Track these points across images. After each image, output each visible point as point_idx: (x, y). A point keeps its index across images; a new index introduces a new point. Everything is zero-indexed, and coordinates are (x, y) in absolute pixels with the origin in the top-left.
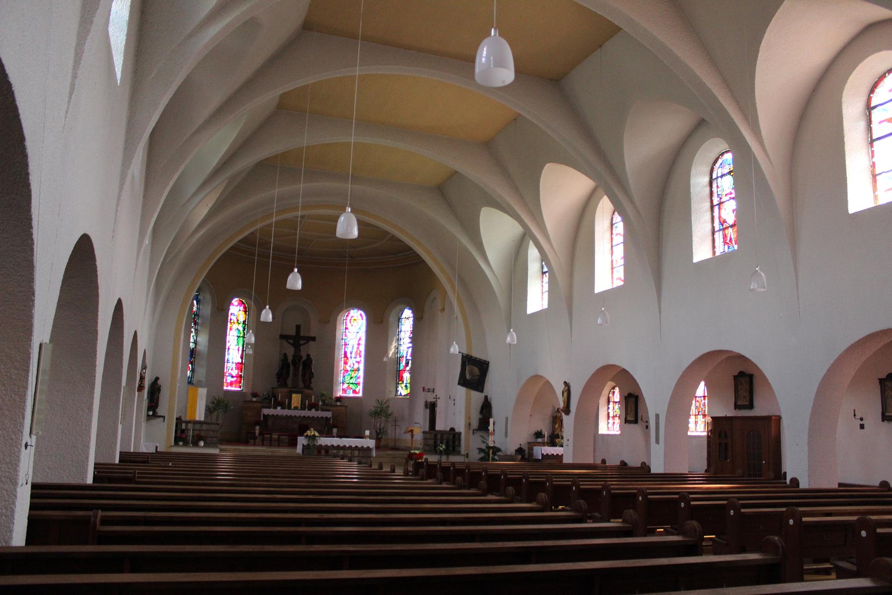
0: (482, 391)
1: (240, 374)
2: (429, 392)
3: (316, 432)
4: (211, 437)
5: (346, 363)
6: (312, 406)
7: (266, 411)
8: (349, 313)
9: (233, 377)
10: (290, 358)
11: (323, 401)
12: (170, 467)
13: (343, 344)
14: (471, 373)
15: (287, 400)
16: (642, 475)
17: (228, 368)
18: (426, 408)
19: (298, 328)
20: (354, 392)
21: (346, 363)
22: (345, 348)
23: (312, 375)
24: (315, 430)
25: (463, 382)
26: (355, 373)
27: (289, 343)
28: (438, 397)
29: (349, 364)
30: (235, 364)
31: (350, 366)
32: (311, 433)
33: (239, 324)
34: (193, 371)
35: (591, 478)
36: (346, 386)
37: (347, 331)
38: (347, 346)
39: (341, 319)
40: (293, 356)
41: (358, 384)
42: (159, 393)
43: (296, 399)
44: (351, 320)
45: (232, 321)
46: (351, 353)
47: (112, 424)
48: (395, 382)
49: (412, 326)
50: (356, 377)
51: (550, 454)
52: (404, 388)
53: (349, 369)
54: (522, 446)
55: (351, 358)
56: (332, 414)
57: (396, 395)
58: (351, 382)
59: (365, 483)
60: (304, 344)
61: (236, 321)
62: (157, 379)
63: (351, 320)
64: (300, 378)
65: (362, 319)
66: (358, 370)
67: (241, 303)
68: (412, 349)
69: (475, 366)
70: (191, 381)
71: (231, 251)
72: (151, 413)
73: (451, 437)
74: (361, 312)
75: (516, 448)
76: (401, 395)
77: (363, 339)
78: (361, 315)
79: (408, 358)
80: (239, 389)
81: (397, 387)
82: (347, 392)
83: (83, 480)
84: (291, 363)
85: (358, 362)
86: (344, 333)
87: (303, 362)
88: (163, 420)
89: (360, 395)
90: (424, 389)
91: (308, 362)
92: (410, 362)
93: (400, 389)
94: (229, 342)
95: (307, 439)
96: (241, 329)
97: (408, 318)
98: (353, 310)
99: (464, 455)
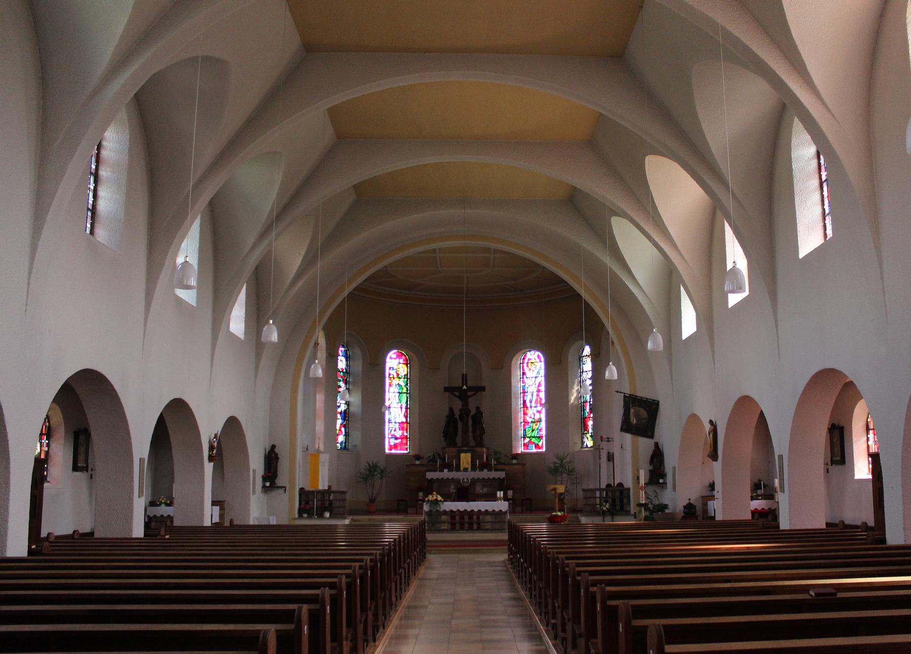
0: (652, 437)
1: (405, 434)
3: (439, 496)
4: (338, 507)
5: (525, 414)
6: (482, 467)
7: (430, 475)
8: (525, 356)
9: (396, 438)
10: (457, 414)
11: (497, 460)
12: (167, 539)
13: (522, 392)
14: (637, 415)
15: (454, 461)
17: (391, 429)
19: (464, 378)
20: (537, 446)
21: (525, 414)
23: (483, 431)
24: (439, 493)
25: (627, 427)
26: (536, 425)
27: (455, 396)
28: (601, 447)
29: (529, 415)
30: (398, 424)
31: (530, 417)
32: (433, 497)
33: (400, 378)
34: (346, 435)
35: (663, 538)
36: (527, 440)
37: (525, 376)
38: (526, 394)
39: (516, 362)
41: (540, 437)
42: (277, 462)
43: (466, 459)
44: (528, 363)
45: (391, 376)
46: (531, 402)
50: (538, 429)
51: (165, 516)
53: (529, 420)
54: (691, 502)
55: (531, 407)
57: (582, 448)
58: (533, 435)
59: (351, 550)
61: (395, 376)
62: (273, 447)
63: (528, 363)
64: (471, 434)
65: (541, 361)
66: (540, 420)
67: (400, 354)
69: (641, 407)
70: (346, 445)
72: (268, 484)
73: (618, 494)
74: (537, 353)
75: (685, 504)
76: (587, 447)
77: (543, 383)
78: (538, 356)
80: (406, 452)
81: (582, 438)
82: (529, 448)
83: (3, 555)
84: (458, 418)
85: (539, 412)
86: (521, 379)
87: (472, 416)
88: (283, 491)
91: (478, 418)
93: (585, 440)
94: (389, 399)
95: (429, 504)
96: (403, 384)
98: (530, 351)
99: (632, 515)
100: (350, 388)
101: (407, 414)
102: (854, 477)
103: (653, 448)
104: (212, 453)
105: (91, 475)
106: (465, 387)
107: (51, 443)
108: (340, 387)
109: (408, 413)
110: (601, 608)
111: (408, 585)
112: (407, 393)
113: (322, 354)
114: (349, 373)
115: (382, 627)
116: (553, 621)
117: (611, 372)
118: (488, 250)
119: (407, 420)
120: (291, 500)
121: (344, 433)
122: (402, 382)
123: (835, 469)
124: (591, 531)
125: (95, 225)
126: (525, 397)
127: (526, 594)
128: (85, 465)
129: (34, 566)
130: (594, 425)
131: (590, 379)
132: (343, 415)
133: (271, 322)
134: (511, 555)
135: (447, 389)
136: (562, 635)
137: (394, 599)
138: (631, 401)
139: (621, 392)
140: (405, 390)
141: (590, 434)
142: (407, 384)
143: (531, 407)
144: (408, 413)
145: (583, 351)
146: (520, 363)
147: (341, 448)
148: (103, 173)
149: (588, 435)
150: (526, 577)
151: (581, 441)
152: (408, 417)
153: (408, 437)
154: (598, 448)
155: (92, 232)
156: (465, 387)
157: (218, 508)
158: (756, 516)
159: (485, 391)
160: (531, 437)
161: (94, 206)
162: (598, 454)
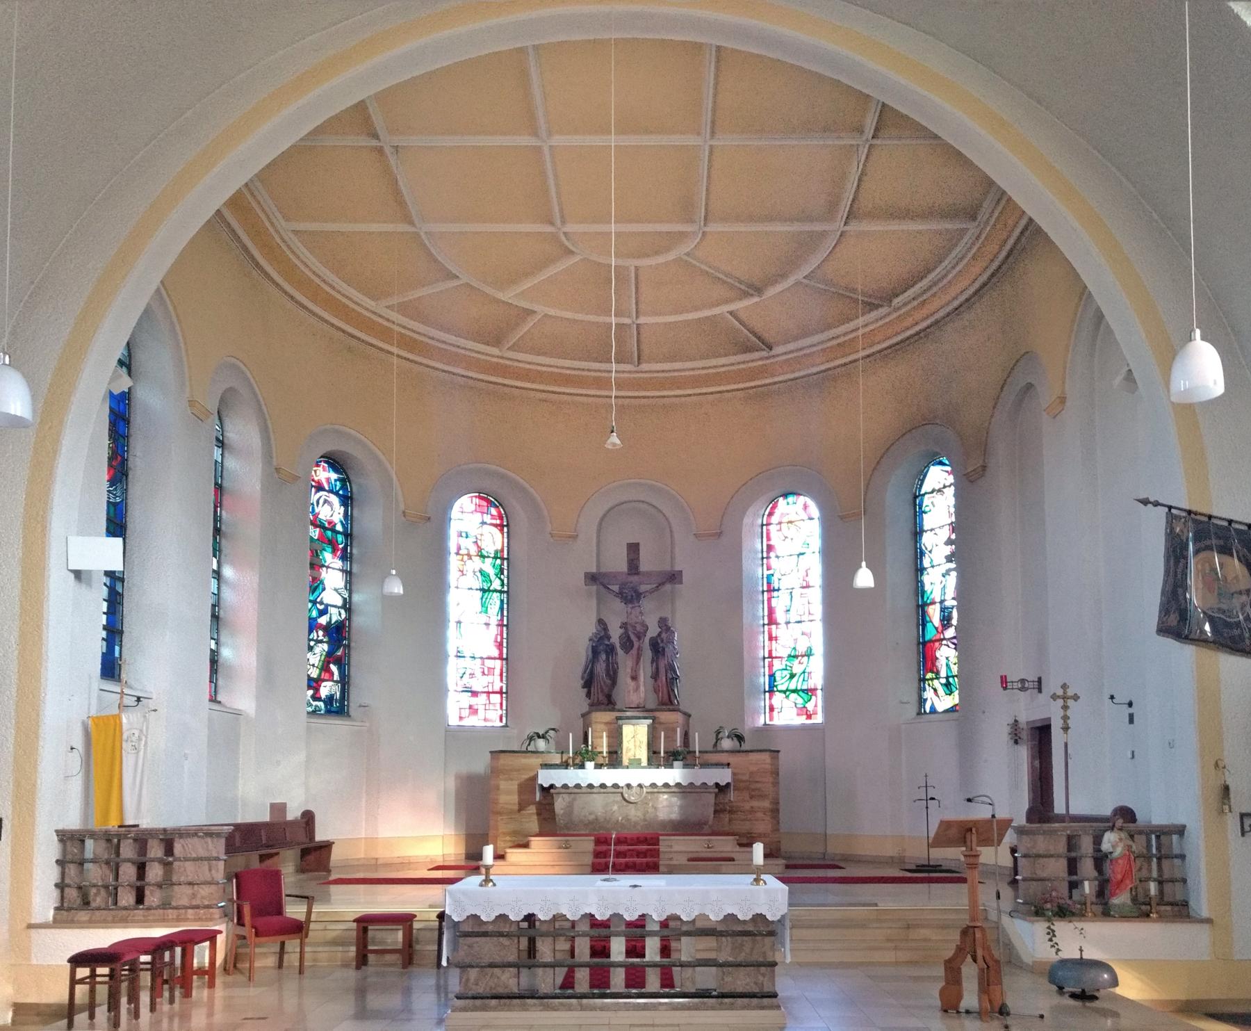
2: (1023, 689)
4: (190, 884)
8: (774, 507)
10: (615, 634)
13: (765, 589)
18: (1016, 742)
22: (769, 600)
28: (1070, 693)
30: (478, 661)
34: (344, 682)
37: (772, 554)
38: (775, 594)
43: (635, 736)
48: (916, 676)
49: (952, 510)
52: (941, 691)
56: (734, 774)
57: (919, 713)
58: (792, 687)
60: (651, 591)
61: (473, 551)
66: (809, 654)
68: (958, 578)
76: (933, 710)
79: (948, 604)
81: (921, 690)
84: (618, 645)
86: (765, 560)
87: (652, 639)
89: (818, 719)
90: (1004, 681)
92: (955, 614)
93: (928, 694)
96: (492, 572)
97: (939, 490)
100: (354, 570)
101: (502, 638)
109: (505, 636)
112: (501, 592)
114: (351, 535)
119: (501, 653)
121: (336, 677)
122: (488, 566)
126: (773, 601)
139: (1156, 504)
140: (496, 584)
141: (944, 681)
143: (788, 623)
144: (505, 636)
145: (923, 481)
146: (762, 525)
147: (329, 712)
151: (915, 697)
152: (505, 645)
153: (504, 690)
159: (682, 583)
160: (787, 690)
162: (1062, 713)
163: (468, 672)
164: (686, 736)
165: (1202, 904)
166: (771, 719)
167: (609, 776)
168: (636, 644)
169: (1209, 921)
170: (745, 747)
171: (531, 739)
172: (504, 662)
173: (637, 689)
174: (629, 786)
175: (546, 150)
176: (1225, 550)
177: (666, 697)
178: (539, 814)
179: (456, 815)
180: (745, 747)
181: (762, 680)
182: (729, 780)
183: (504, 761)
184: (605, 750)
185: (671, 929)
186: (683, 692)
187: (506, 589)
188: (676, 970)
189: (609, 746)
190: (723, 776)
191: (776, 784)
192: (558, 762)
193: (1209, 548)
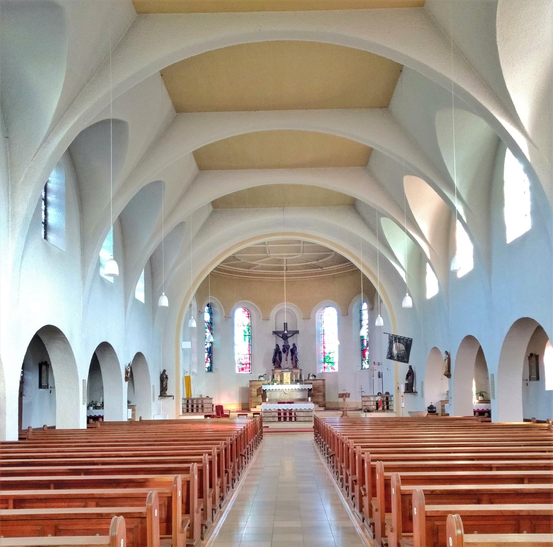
0: (407, 362)
9: (243, 364)
10: (281, 348)
16: (34, 440)
18: (379, 377)
19: (286, 325)
27: (280, 336)
28: (374, 369)
40: (283, 346)
43: (287, 376)
47: (76, 404)
54: (433, 404)
56: (313, 386)
57: (362, 369)
60: (290, 337)
62: (164, 371)
67: (244, 310)
71: (214, 271)
76: (365, 369)
81: (362, 363)
87: (291, 349)
89: (337, 370)
90: (374, 363)
93: (364, 364)
96: (247, 330)
102: (545, 389)
103: (408, 369)
104: (128, 376)
105: (51, 391)
106: (286, 332)
107: (24, 371)
108: (206, 332)
110: (367, 466)
111: (252, 455)
112: (249, 336)
113: (195, 312)
115: (237, 480)
116: (341, 476)
117: (380, 321)
118: (299, 242)
119: (249, 353)
120: (177, 403)
121: (209, 362)
123: (533, 383)
124: (368, 421)
125: (47, 232)
127: (325, 461)
128: (47, 385)
129: (23, 446)
130: (369, 355)
131: (367, 325)
132: (209, 350)
133: (164, 294)
134: (316, 437)
135: (275, 333)
136: (346, 484)
137: (244, 463)
138: (394, 339)
139: (387, 333)
140: (248, 334)
141: (367, 361)
142: (249, 330)
148: (49, 198)
149: (366, 361)
150: (325, 450)
151: (361, 365)
154: (372, 369)
155: (45, 237)
156: (286, 332)
157: (131, 410)
158: (477, 414)
161: (46, 220)
163: (241, 358)
164: (301, 375)
165: (395, 410)
166: (324, 370)
167: (280, 387)
168: (287, 351)
169: (396, 412)
170: (316, 378)
171: (260, 377)
172: (250, 337)
173: (287, 363)
174: (286, 389)
175: (267, 247)
176: (399, 342)
177: (295, 366)
178: (262, 397)
179: (476, 362)
180: (316, 378)
181: (321, 359)
182: (312, 388)
183: (253, 383)
184: (279, 380)
185: (296, 410)
186: (300, 364)
187: (250, 335)
188: (291, 367)
189: (280, 379)
190: (310, 387)
191: (324, 388)
192: (267, 383)
193: (396, 342)
